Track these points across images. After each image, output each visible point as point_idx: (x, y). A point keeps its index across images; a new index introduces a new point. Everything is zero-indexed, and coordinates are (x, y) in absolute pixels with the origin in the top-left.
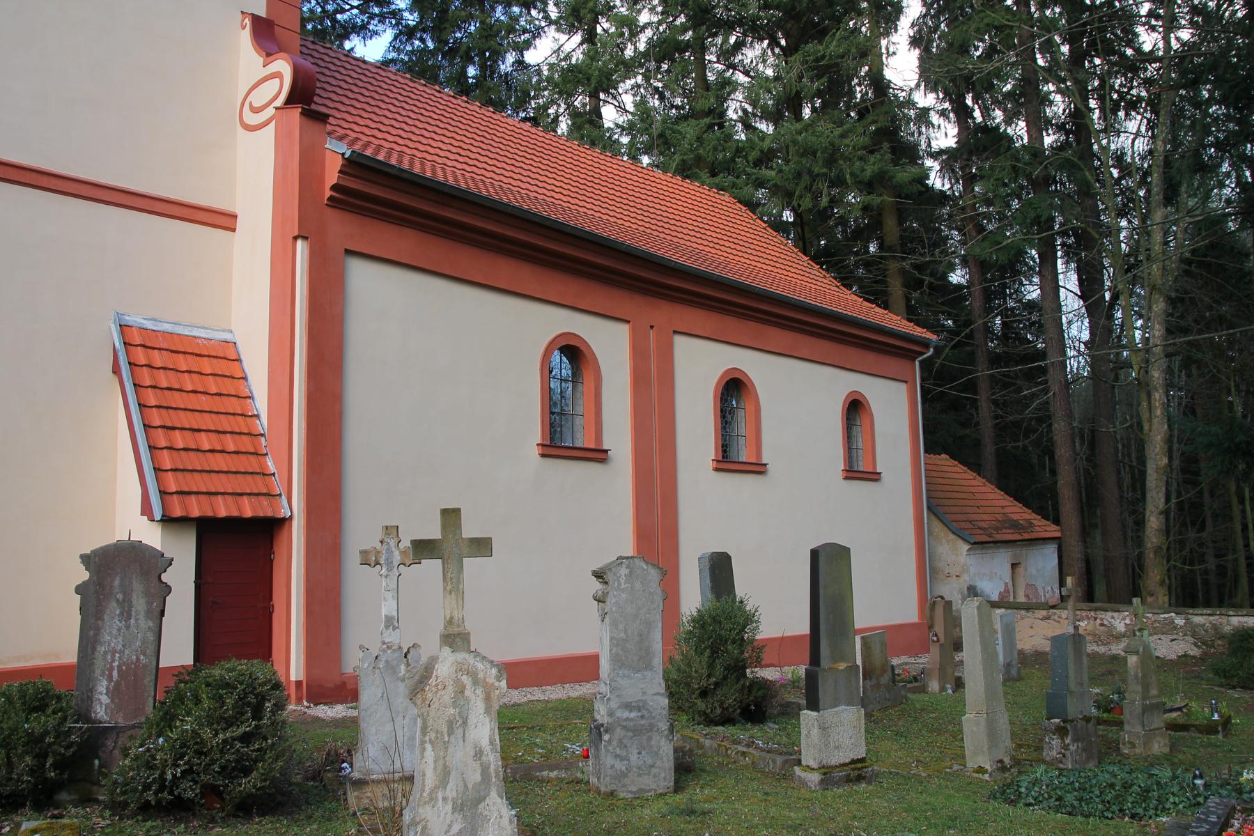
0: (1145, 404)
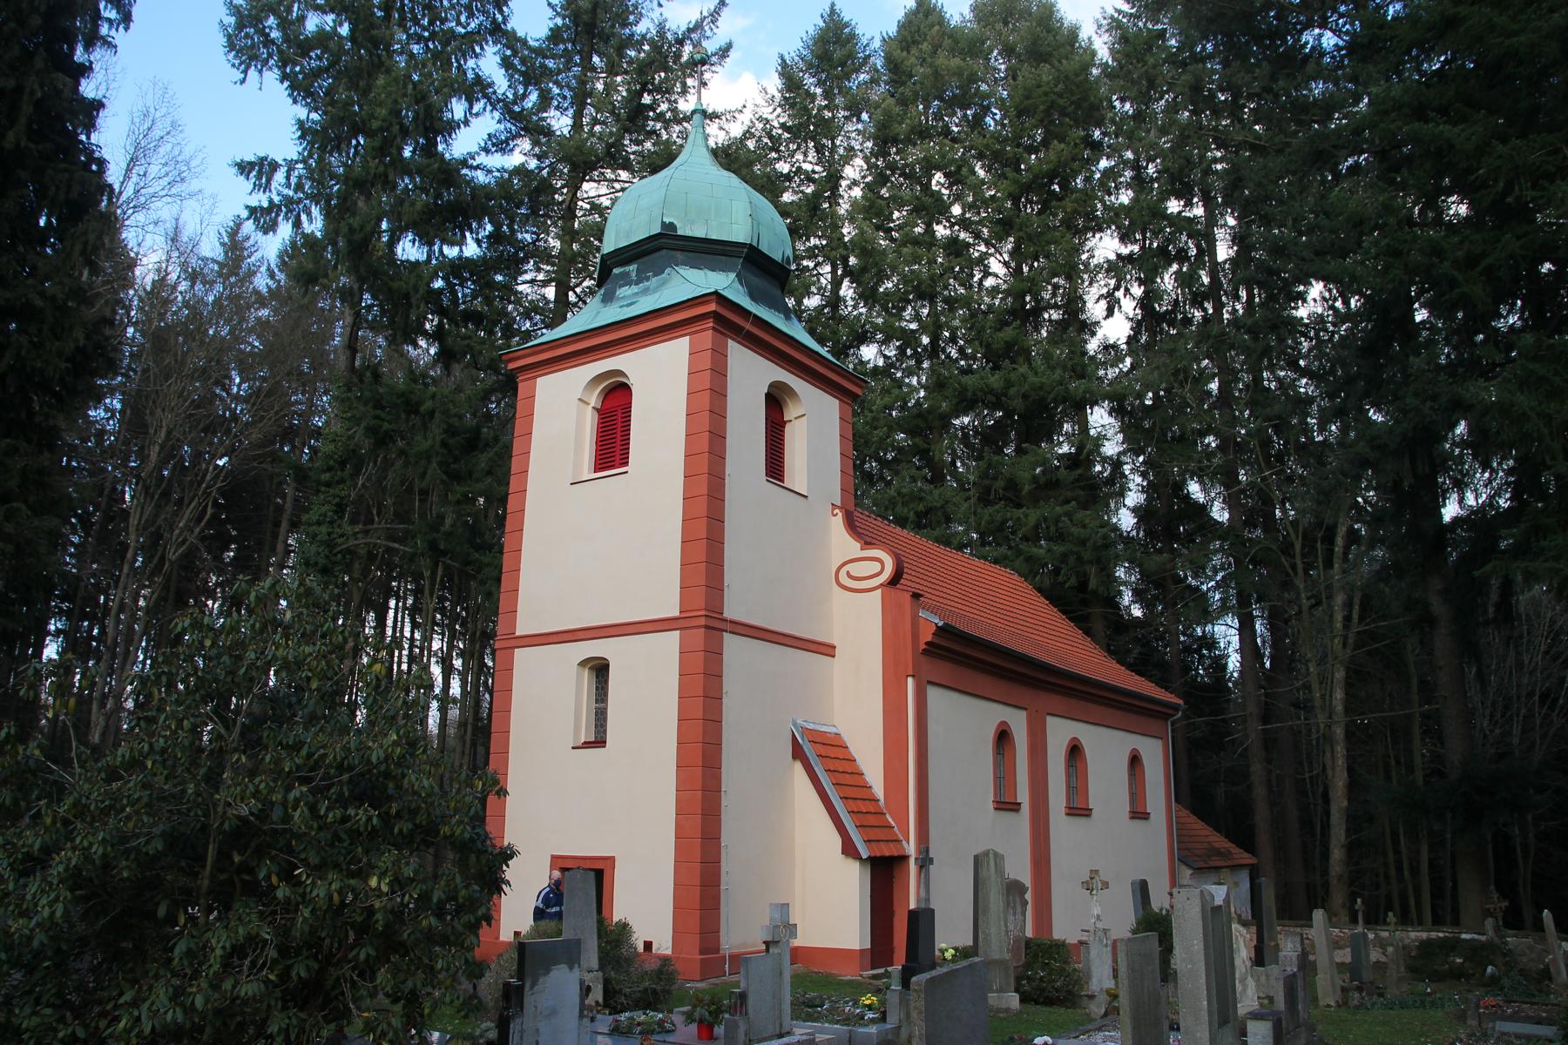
0: (1328, 755)
